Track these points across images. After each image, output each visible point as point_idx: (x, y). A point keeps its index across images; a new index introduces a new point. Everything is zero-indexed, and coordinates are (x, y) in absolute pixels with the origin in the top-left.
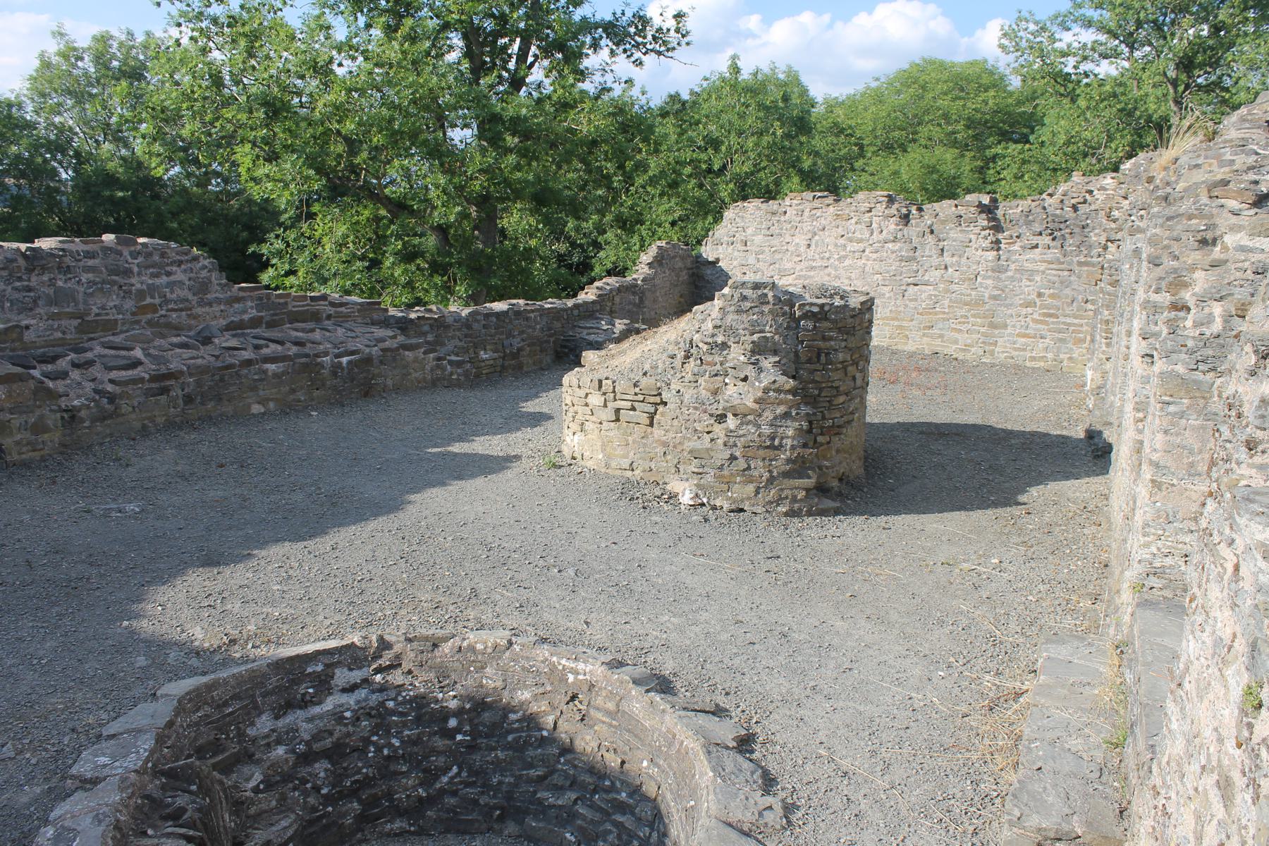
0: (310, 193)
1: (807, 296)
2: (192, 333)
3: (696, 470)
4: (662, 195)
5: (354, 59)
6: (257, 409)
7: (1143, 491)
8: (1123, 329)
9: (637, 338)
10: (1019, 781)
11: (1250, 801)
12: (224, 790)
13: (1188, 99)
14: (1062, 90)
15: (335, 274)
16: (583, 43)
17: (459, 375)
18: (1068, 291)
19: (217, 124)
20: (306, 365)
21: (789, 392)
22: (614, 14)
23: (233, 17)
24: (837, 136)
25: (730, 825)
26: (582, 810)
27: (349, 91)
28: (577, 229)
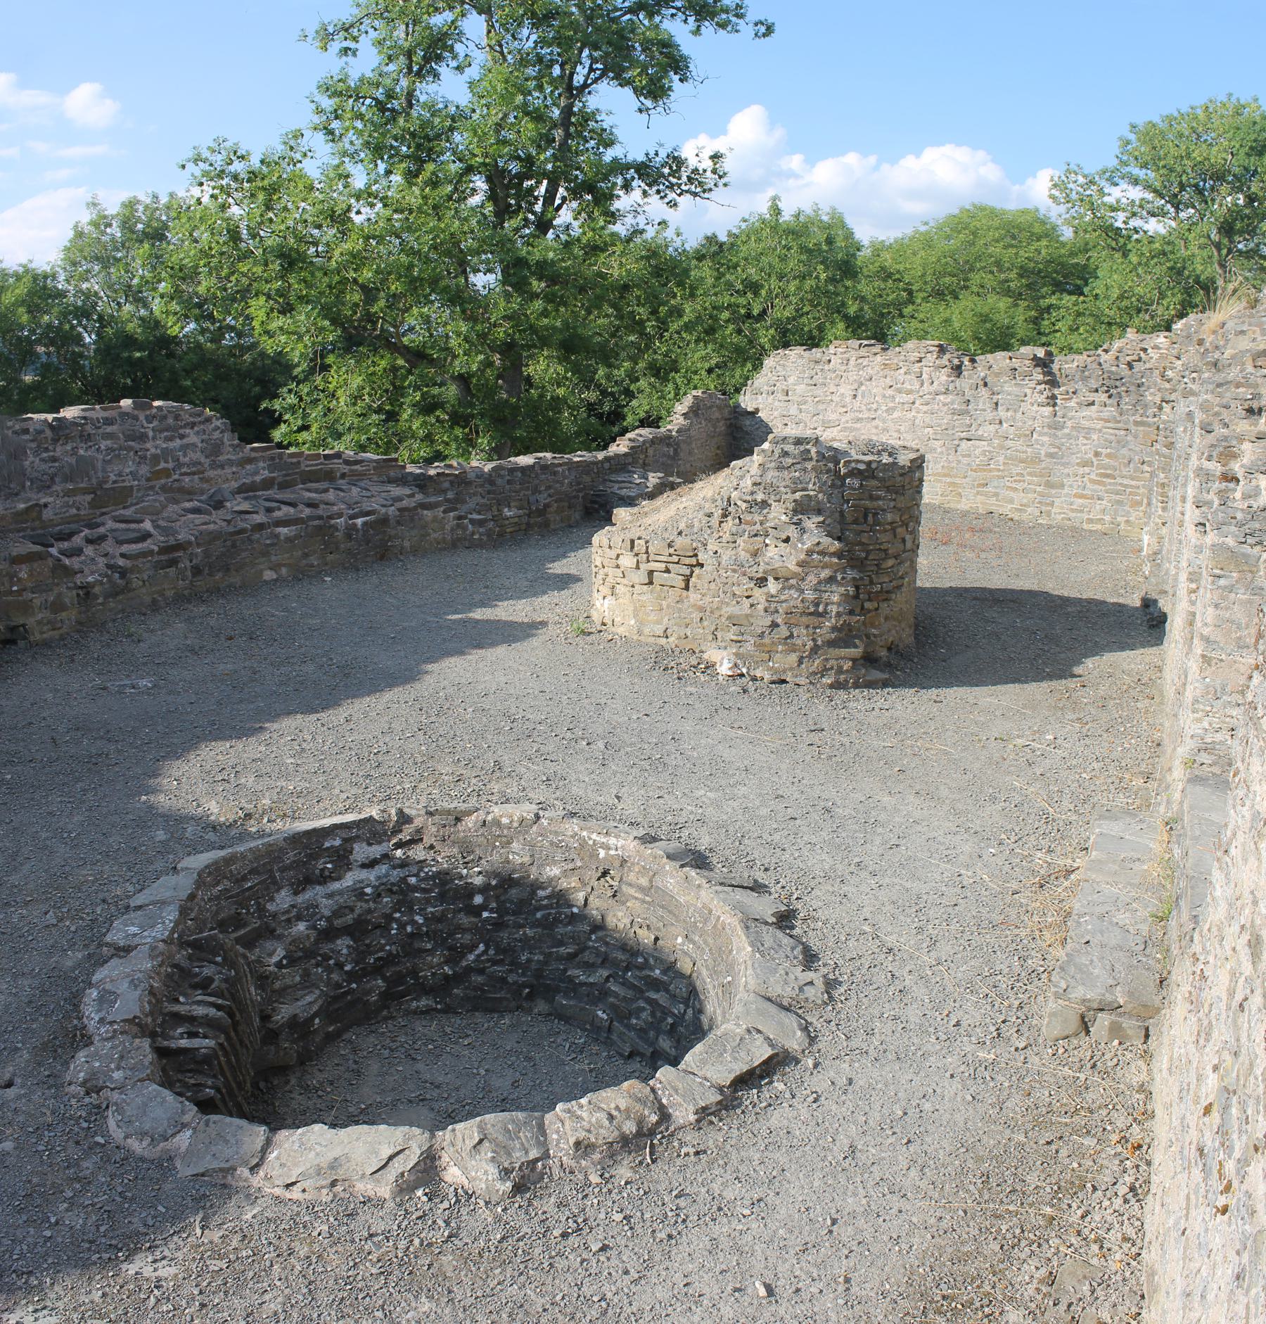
0: (322, 344)
1: (853, 452)
3: (735, 638)
4: (697, 341)
5: (372, 205)
6: (269, 575)
9: (672, 494)
12: (248, 964)
13: (1232, 264)
14: (1114, 244)
15: (349, 429)
16: (615, 184)
17: (481, 535)
18: (1124, 451)
19: (233, 279)
20: (319, 528)
22: (647, 155)
24: (885, 280)
25: (769, 999)
27: (367, 238)
28: (608, 377)
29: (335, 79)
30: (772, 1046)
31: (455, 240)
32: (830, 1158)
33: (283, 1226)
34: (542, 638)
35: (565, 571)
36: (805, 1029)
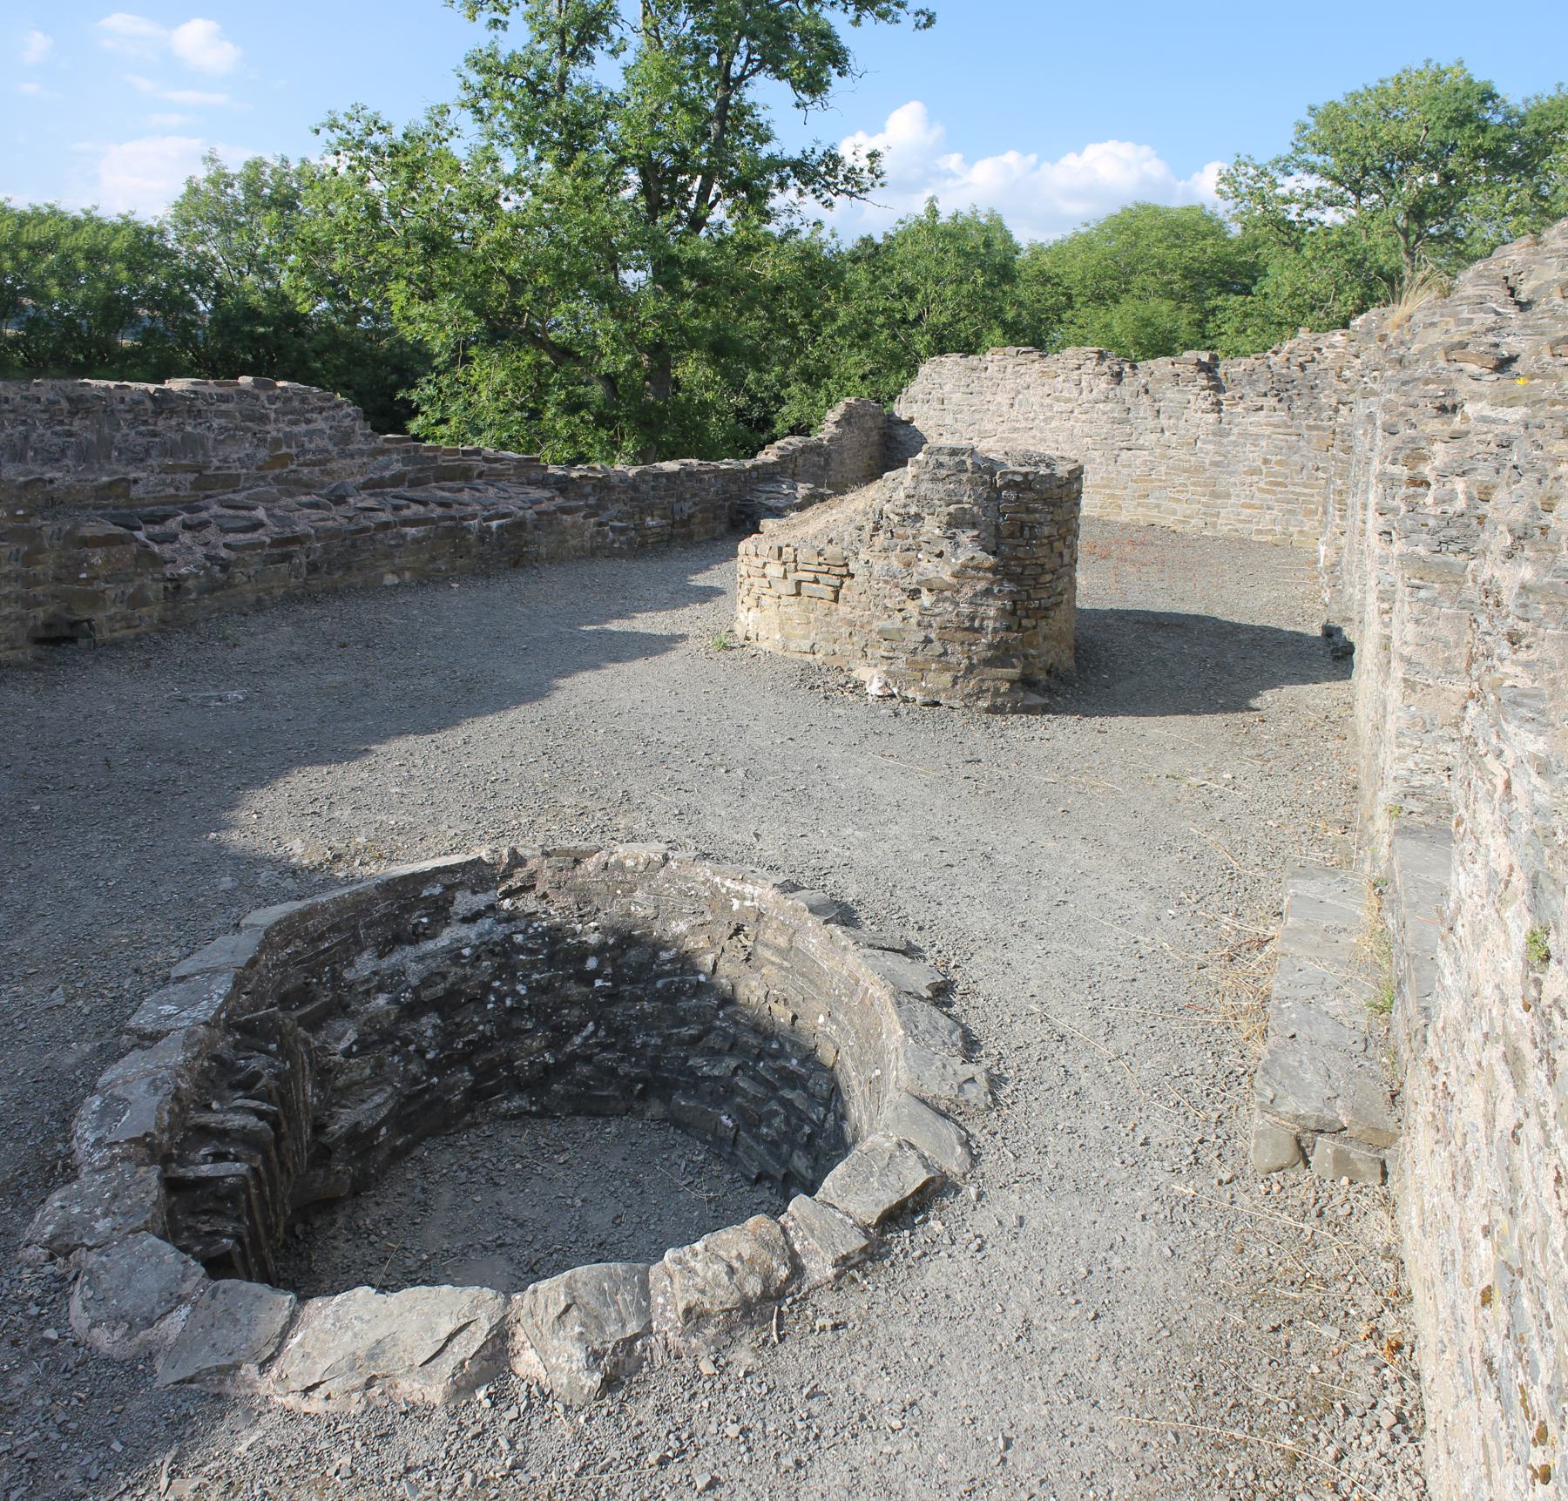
0: (465, 335)
1: (1009, 464)
2: (323, 492)
4: (851, 346)
5: (521, 193)
6: (390, 579)
7: (1394, 693)
8: (1358, 501)
10: (1270, 1052)
11: (1545, 1080)
12: (309, 1053)
14: (1286, 239)
16: (770, 182)
18: (1296, 458)
19: (371, 258)
20: (451, 529)
21: (988, 569)
23: (395, 146)
24: (1043, 284)
25: (923, 1101)
26: (743, 1083)
27: (515, 227)
28: (758, 382)
29: (485, 53)
30: (927, 1167)
31: (605, 234)
32: (999, 1338)
33: (289, 1461)
34: (682, 652)
35: (708, 583)
36: (966, 1144)
